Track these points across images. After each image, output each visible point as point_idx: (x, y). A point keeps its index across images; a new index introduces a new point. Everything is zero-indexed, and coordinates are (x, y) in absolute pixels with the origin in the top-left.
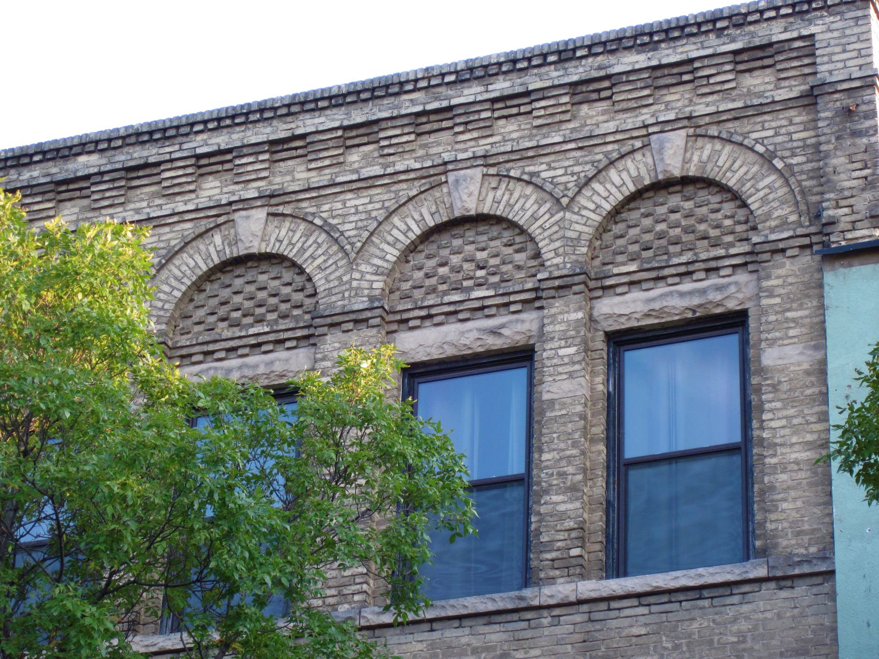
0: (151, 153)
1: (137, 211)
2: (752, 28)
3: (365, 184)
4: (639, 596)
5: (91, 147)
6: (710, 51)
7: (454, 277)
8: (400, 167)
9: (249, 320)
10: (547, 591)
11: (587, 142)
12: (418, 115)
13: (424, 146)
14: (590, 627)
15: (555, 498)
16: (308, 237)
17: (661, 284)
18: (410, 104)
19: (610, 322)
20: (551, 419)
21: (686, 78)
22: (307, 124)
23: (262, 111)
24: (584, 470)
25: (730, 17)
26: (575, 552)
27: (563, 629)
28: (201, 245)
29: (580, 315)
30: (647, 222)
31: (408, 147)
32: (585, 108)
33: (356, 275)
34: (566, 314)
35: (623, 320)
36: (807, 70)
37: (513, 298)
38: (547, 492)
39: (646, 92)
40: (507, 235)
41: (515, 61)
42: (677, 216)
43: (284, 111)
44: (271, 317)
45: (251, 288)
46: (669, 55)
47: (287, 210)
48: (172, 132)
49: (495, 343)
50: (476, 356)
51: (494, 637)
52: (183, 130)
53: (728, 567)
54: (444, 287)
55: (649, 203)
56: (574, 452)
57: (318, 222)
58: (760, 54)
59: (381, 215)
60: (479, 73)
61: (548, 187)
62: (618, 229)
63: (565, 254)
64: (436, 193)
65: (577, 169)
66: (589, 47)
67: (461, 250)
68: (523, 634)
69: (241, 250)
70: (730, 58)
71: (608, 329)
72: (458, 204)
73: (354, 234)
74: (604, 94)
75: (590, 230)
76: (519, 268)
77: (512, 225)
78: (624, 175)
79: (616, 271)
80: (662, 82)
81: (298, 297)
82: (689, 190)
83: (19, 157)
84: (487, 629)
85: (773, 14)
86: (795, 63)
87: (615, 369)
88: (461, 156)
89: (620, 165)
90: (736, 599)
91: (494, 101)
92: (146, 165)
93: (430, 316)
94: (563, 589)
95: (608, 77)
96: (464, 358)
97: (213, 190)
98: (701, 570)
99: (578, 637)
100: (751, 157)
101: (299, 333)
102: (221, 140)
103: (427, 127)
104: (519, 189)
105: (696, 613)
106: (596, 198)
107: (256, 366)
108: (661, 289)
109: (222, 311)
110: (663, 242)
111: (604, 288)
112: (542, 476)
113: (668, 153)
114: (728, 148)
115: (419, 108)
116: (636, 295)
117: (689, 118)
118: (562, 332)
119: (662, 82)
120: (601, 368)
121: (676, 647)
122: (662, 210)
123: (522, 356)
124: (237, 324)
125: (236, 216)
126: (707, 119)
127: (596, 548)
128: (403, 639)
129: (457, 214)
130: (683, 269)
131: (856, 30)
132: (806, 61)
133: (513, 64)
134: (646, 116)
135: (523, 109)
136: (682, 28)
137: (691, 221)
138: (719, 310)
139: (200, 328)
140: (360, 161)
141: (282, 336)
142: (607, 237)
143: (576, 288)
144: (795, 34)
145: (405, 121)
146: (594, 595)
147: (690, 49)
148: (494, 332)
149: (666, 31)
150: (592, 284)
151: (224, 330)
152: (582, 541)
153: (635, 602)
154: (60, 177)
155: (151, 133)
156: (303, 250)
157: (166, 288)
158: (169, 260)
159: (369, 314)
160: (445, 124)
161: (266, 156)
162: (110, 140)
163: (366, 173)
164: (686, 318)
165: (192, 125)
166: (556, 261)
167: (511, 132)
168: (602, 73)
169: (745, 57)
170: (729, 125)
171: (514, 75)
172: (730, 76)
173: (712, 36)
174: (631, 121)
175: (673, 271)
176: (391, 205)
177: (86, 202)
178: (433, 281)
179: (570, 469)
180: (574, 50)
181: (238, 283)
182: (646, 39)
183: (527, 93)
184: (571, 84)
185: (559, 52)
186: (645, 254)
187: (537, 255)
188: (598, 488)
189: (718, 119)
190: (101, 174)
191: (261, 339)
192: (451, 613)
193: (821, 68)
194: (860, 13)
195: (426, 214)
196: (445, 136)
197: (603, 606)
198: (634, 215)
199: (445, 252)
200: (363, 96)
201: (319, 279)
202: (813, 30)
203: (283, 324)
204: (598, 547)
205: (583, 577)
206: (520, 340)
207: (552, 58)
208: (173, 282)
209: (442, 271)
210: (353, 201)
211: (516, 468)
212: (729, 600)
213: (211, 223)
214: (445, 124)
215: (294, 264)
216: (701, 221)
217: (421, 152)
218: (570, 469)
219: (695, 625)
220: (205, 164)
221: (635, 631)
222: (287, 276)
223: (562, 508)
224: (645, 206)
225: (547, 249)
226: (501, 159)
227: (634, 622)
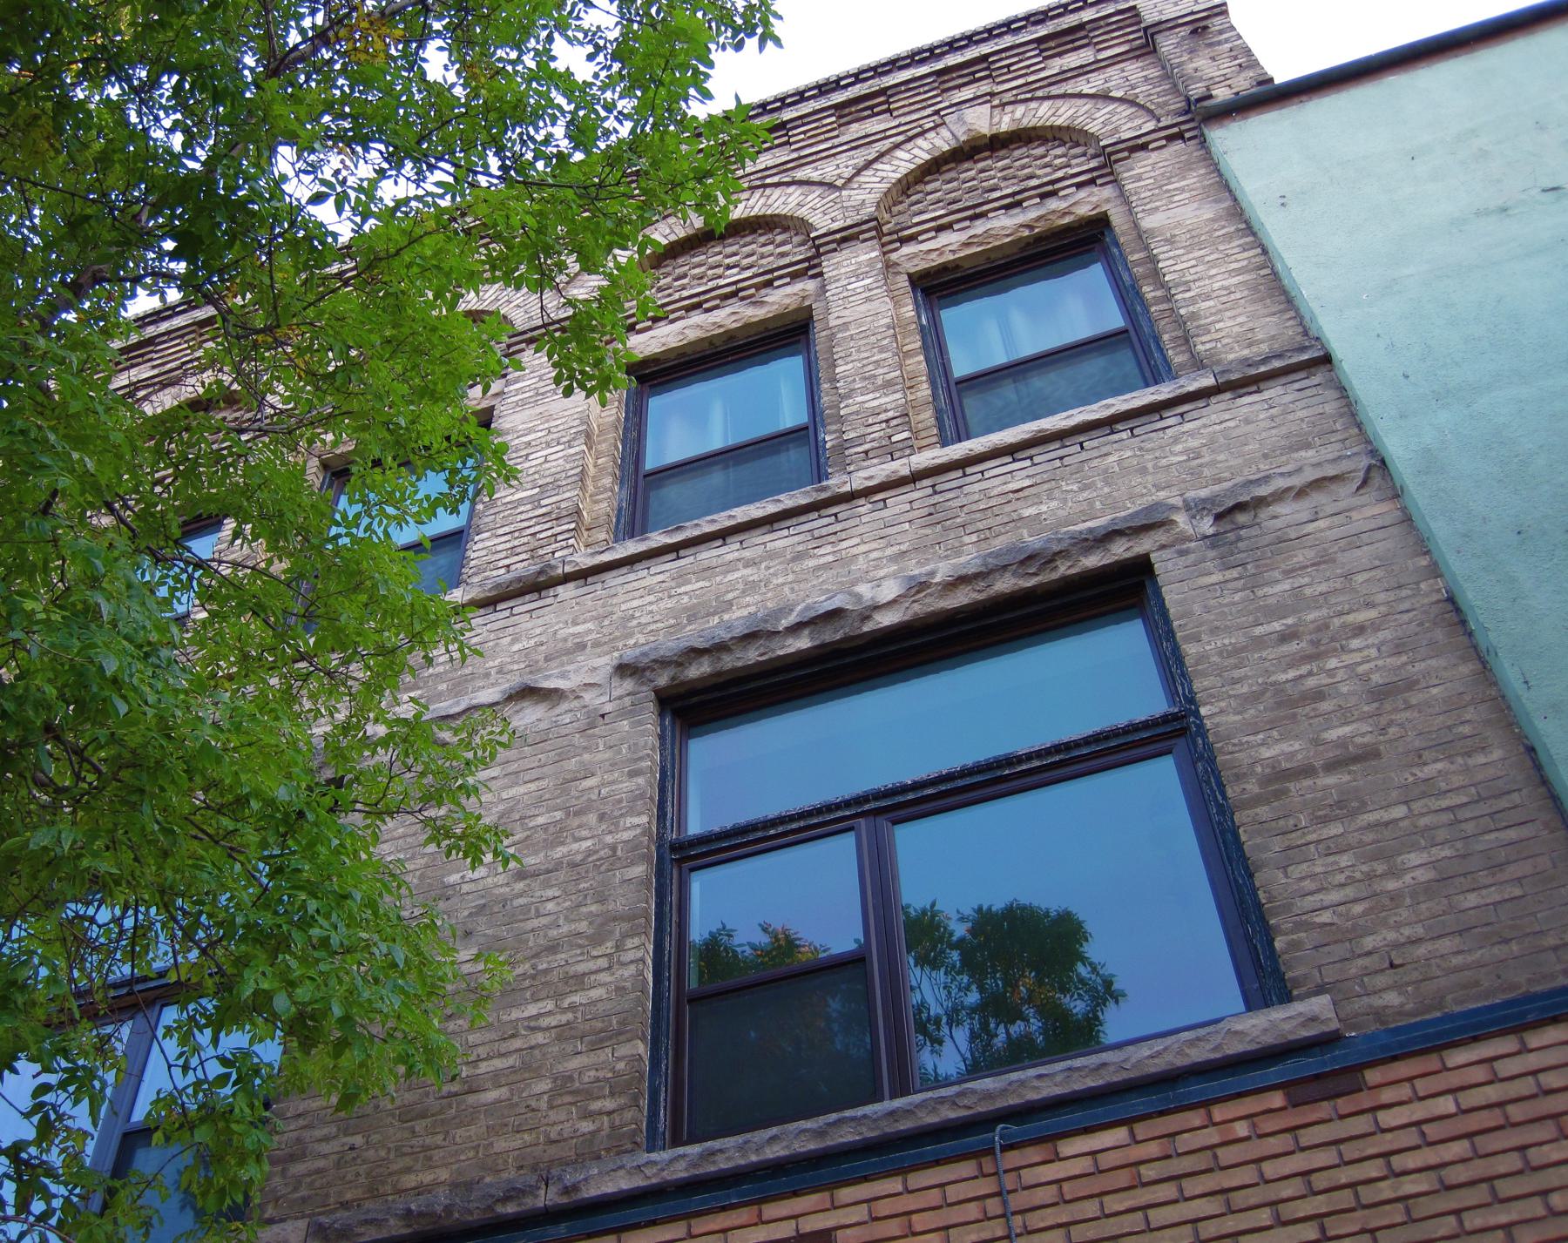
19: (916, 261)
35: (934, 255)
71: (912, 270)
127: (642, 1138)
138: (1067, 220)
164: (1021, 238)
192: (708, 529)
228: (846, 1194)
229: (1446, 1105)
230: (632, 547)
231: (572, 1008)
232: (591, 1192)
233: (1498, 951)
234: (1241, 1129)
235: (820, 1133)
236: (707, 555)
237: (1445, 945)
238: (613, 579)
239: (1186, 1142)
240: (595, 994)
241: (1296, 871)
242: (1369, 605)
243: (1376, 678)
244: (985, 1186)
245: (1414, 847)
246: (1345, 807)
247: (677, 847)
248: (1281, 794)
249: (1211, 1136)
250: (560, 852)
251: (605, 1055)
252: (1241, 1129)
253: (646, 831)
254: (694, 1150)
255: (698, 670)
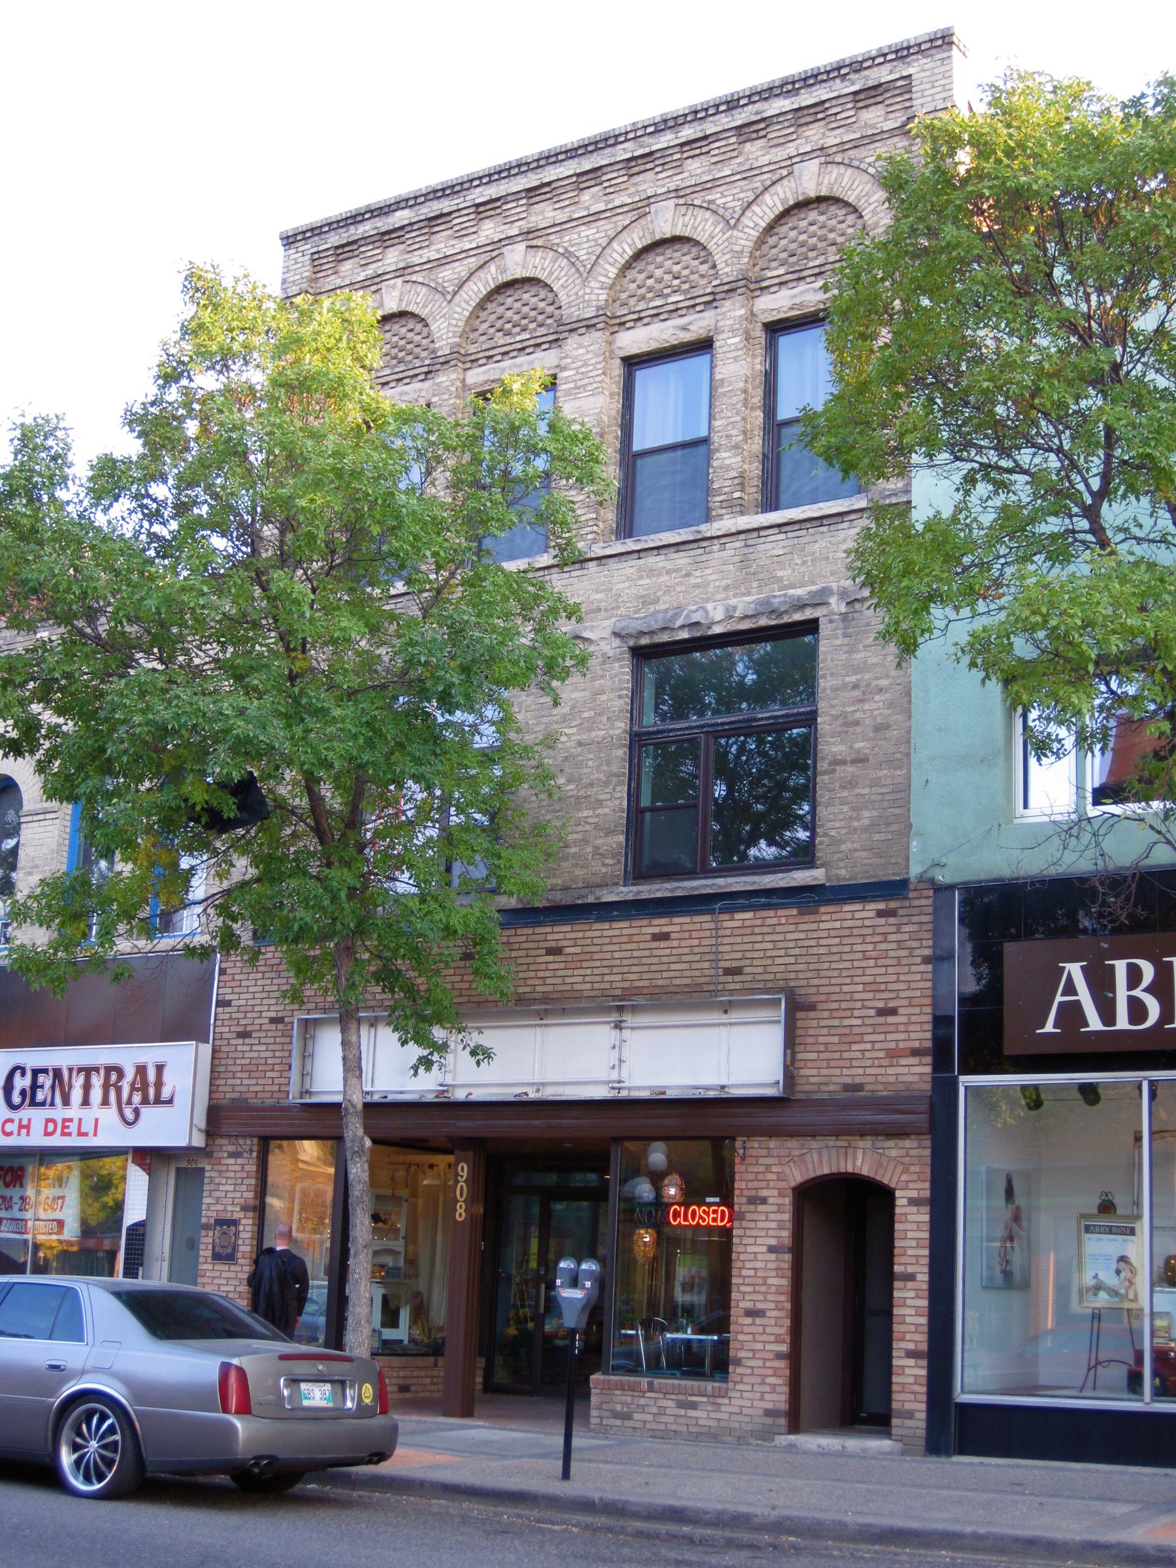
0: (444, 205)
1: (438, 251)
2: (866, 73)
3: (593, 218)
4: (779, 526)
5: (403, 204)
6: (835, 94)
7: (658, 286)
8: (617, 203)
9: (517, 329)
10: (716, 525)
11: (748, 174)
12: (629, 160)
13: (635, 184)
14: (746, 550)
15: (724, 455)
16: (554, 262)
17: (802, 283)
18: (623, 152)
20: (724, 394)
21: (820, 116)
22: (551, 173)
23: (519, 166)
24: (745, 433)
25: (850, 65)
26: (737, 495)
27: (729, 552)
28: (481, 274)
29: (743, 312)
30: (793, 234)
31: (623, 186)
32: (748, 145)
33: (588, 290)
34: (733, 311)
36: (907, 104)
37: (698, 301)
38: (718, 450)
39: (791, 130)
40: (694, 250)
41: (696, 112)
42: (814, 228)
43: (534, 165)
44: (532, 326)
45: (518, 305)
46: (806, 98)
47: (539, 242)
48: (457, 188)
49: (686, 337)
50: (674, 347)
51: (681, 561)
52: (466, 186)
53: (840, 501)
54: (650, 295)
55: (795, 218)
56: (738, 418)
57: (561, 250)
58: (873, 93)
59: (604, 242)
60: (671, 123)
61: (721, 211)
62: (772, 241)
63: (733, 264)
64: (643, 221)
65: (741, 195)
66: (749, 96)
67: (664, 264)
68: (699, 559)
69: (508, 277)
70: (850, 98)
72: (657, 230)
73: (582, 262)
74: (762, 133)
75: (751, 244)
76: (702, 276)
77: (697, 243)
78: (775, 198)
79: (769, 274)
80: (803, 121)
81: (550, 309)
82: (824, 206)
83: (354, 216)
84: (676, 555)
85: (881, 60)
86: (899, 99)
87: (771, 349)
88: (660, 191)
89: (772, 190)
90: (845, 525)
91: (682, 145)
92: (442, 215)
93: (640, 319)
94: (728, 523)
95: (763, 120)
96: (665, 349)
97: (489, 230)
98: (821, 505)
99: (738, 559)
100: (866, 177)
101: (551, 338)
102: (493, 191)
103: (636, 170)
104: (701, 214)
105: (818, 537)
106: (755, 218)
107: (521, 365)
108: (802, 287)
109: (498, 324)
110: (804, 249)
111: (761, 289)
112: (715, 438)
113: (805, 178)
114: (850, 170)
115: (629, 155)
116: (785, 292)
117: (822, 149)
118: (729, 323)
119: (803, 121)
120: (760, 352)
121: (804, 563)
122: (803, 224)
123: (704, 345)
124: (509, 334)
125: (504, 250)
126: (834, 149)
127: (753, 493)
128: (620, 565)
129: (658, 237)
130: (816, 270)
131: (942, 69)
132: (907, 96)
133: (696, 114)
134: (791, 150)
135: (704, 150)
136: (816, 76)
137: (824, 231)
139: (484, 338)
140: (592, 200)
141: (539, 340)
142: (765, 248)
143: (740, 291)
144: (897, 76)
145: (620, 166)
146: (748, 527)
147: (821, 93)
148: (684, 328)
149: (805, 79)
150: (752, 286)
151: (500, 339)
152: (742, 487)
153: (776, 530)
154: (383, 230)
155: (443, 190)
156: (551, 273)
157: (458, 310)
158: (460, 287)
159: (595, 321)
160: (649, 166)
161: (524, 201)
162: (416, 198)
163: (593, 210)
165: (472, 181)
166: (728, 269)
167: (696, 169)
168: (758, 117)
169: (862, 96)
170: (851, 152)
171: (696, 124)
172: (852, 113)
173: (838, 81)
174: (780, 154)
175: (810, 272)
176: (612, 233)
177: (402, 247)
178: (643, 290)
179: (734, 432)
180: (738, 100)
181: (509, 301)
182: (790, 87)
183: (705, 137)
184: (736, 128)
185: (728, 102)
186: (792, 260)
187: (714, 267)
188: (756, 445)
189: (843, 148)
190: (411, 224)
191: (525, 344)
193: (915, 102)
194: (945, 55)
195: (636, 239)
196: (649, 176)
197: (755, 534)
198: (784, 229)
199: (651, 268)
200: (590, 148)
201: (563, 298)
202: (911, 71)
203: (543, 331)
204: (754, 490)
205: (742, 513)
206: (703, 333)
207: (722, 108)
208: (464, 305)
209: (650, 282)
210: (587, 232)
211: (703, 433)
212: (841, 526)
213: (486, 257)
214: (649, 166)
215: (546, 285)
216: (831, 231)
217: (632, 190)
218: (734, 432)
219: (817, 545)
220: (482, 210)
221: (777, 552)
222: (543, 293)
223: (728, 462)
224: (792, 221)
225: (719, 260)
226: (688, 191)
227: (775, 545)
228: (676, 920)
229: (838, 925)
230: (618, 548)
231: (598, 816)
232: (604, 900)
233: (878, 861)
234: (783, 920)
235: (672, 891)
236: (652, 560)
237: (864, 854)
238: (613, 564)
239: (769, 921)
240: (607, 810)
241: (831, 809)
242: (888, 676)
243: (879, 720)
244: (711, 926)
245: (866, 808)
246: (851, 784)
247: (637, 734)
248: (833, 771)
249: (774, 921)
250: (593, 734)
251: (610, 839)
252: (783, 920)
253: (625, 731)
254: (635, 889)
255: (645, 641)
